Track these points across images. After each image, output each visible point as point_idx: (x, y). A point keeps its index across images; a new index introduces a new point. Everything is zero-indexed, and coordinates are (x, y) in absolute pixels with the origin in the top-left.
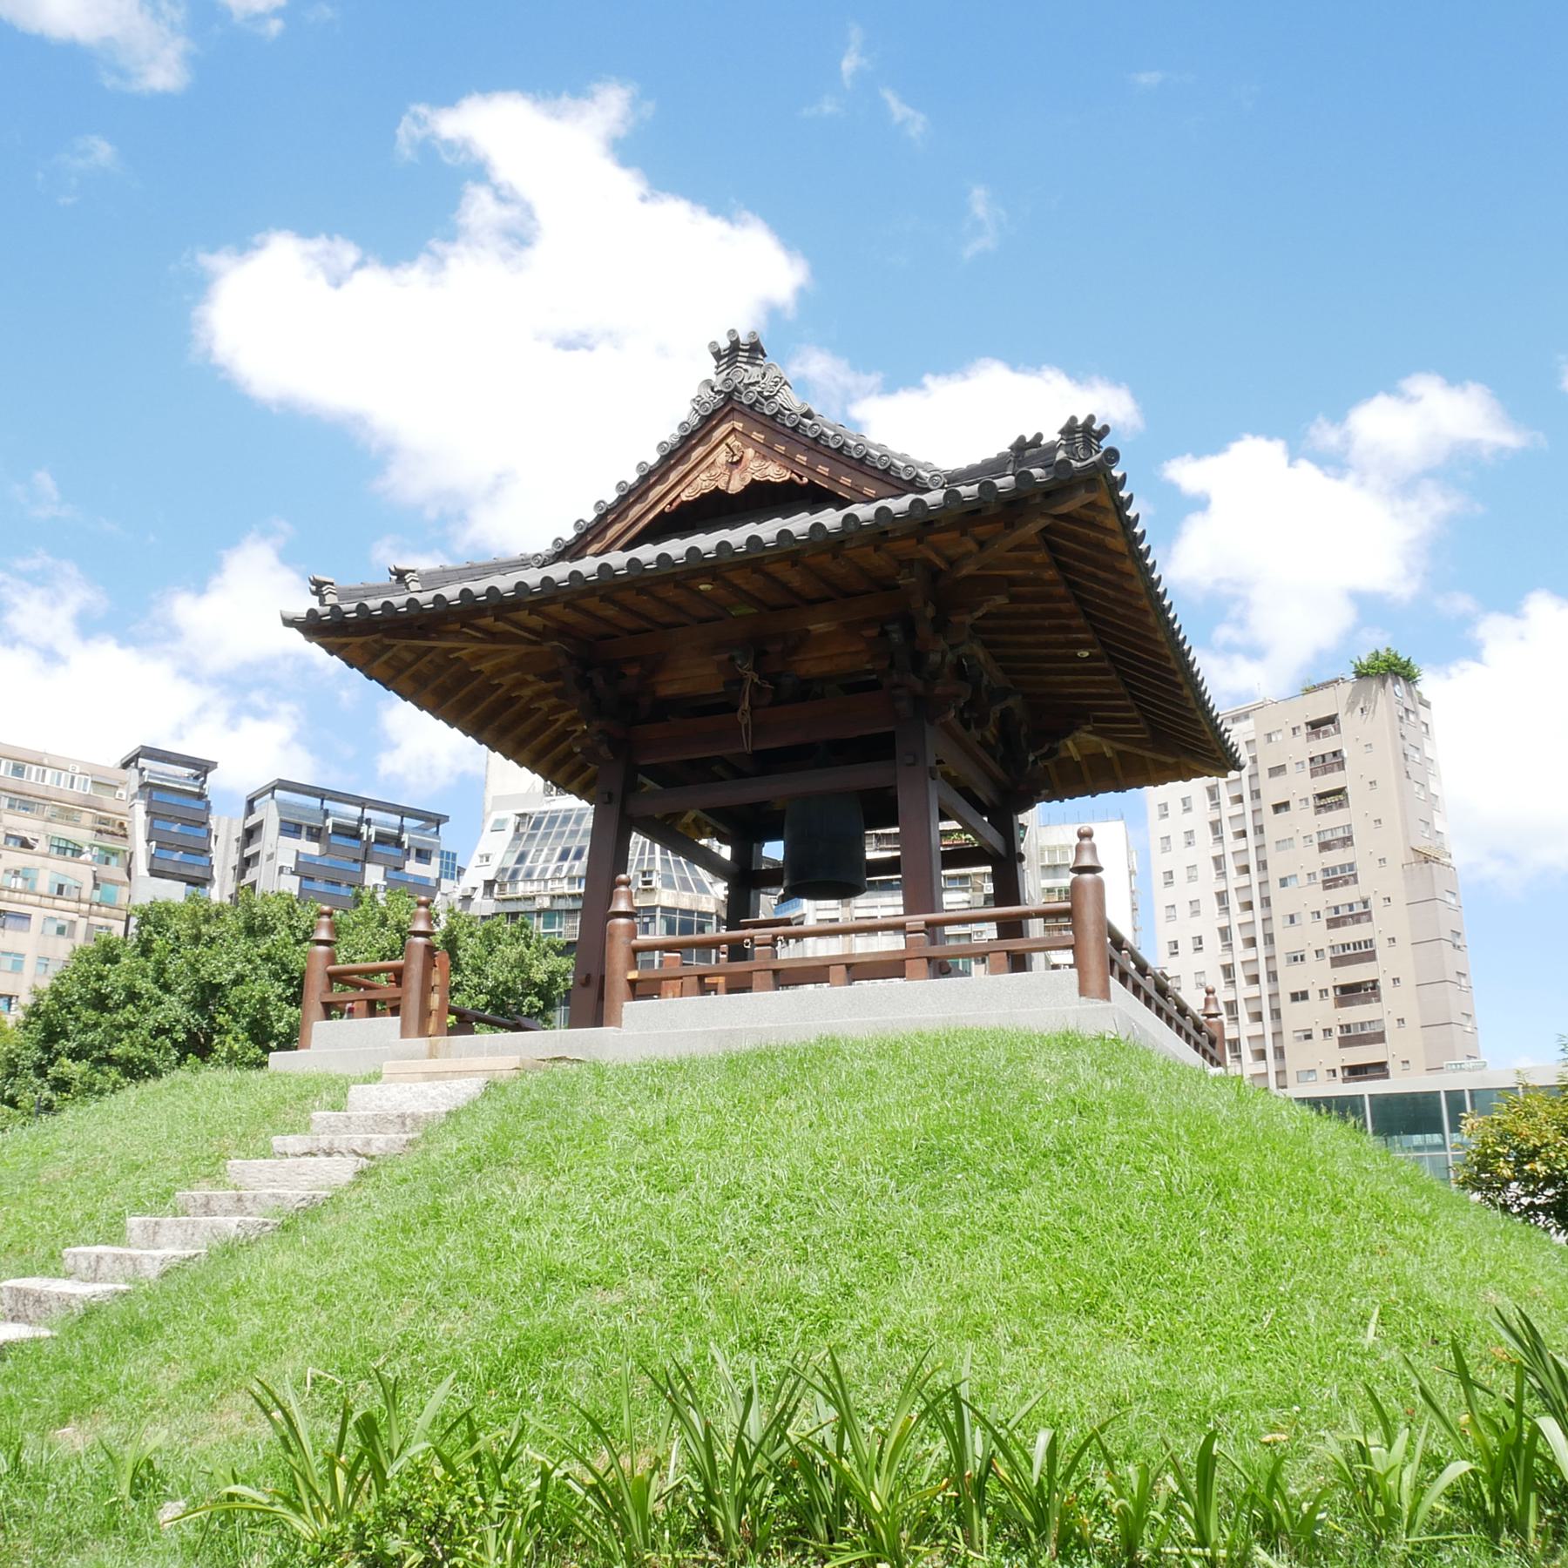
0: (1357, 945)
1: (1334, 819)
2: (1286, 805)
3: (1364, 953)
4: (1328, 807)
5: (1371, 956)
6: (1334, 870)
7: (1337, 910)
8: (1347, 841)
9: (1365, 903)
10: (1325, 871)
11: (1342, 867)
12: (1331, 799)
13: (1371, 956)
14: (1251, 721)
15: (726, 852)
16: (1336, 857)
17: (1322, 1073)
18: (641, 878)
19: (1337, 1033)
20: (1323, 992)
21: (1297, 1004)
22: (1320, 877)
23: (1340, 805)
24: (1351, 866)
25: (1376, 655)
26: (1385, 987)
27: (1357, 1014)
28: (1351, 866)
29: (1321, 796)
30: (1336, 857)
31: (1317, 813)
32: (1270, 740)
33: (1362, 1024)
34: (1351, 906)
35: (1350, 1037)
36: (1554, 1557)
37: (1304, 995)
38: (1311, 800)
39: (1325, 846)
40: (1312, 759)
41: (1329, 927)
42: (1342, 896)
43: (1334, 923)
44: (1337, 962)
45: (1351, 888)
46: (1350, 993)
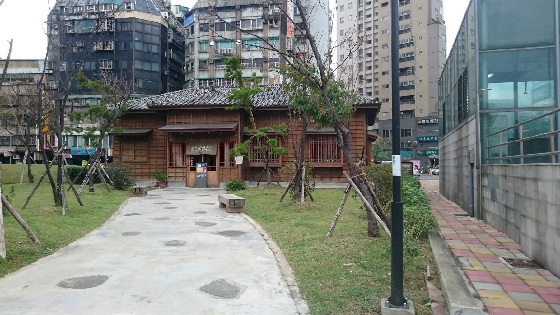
18: (126, 6)
21: (384, 76)
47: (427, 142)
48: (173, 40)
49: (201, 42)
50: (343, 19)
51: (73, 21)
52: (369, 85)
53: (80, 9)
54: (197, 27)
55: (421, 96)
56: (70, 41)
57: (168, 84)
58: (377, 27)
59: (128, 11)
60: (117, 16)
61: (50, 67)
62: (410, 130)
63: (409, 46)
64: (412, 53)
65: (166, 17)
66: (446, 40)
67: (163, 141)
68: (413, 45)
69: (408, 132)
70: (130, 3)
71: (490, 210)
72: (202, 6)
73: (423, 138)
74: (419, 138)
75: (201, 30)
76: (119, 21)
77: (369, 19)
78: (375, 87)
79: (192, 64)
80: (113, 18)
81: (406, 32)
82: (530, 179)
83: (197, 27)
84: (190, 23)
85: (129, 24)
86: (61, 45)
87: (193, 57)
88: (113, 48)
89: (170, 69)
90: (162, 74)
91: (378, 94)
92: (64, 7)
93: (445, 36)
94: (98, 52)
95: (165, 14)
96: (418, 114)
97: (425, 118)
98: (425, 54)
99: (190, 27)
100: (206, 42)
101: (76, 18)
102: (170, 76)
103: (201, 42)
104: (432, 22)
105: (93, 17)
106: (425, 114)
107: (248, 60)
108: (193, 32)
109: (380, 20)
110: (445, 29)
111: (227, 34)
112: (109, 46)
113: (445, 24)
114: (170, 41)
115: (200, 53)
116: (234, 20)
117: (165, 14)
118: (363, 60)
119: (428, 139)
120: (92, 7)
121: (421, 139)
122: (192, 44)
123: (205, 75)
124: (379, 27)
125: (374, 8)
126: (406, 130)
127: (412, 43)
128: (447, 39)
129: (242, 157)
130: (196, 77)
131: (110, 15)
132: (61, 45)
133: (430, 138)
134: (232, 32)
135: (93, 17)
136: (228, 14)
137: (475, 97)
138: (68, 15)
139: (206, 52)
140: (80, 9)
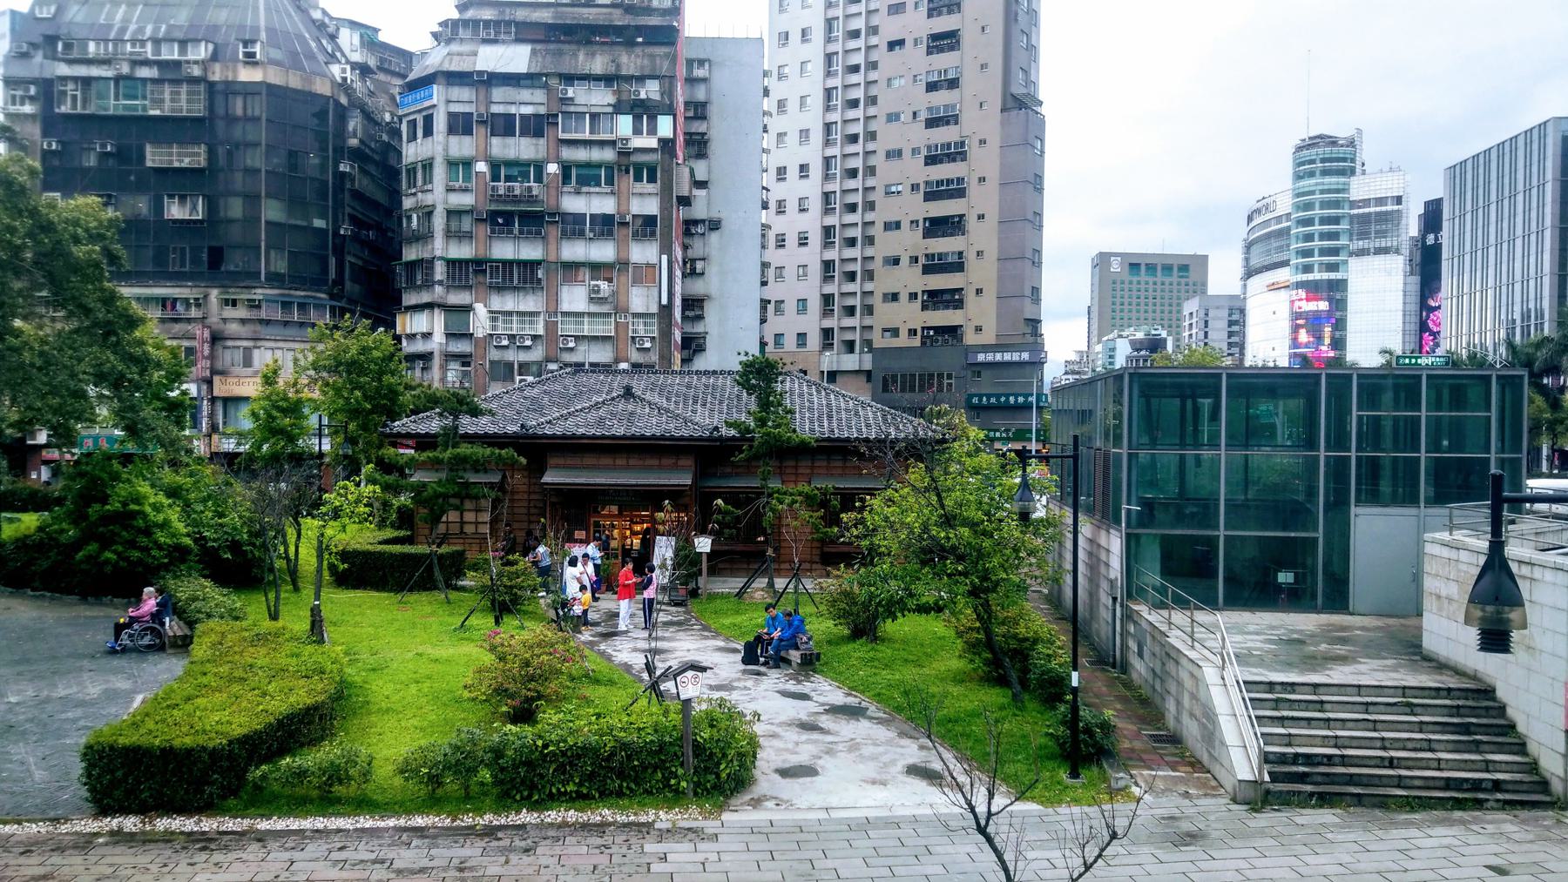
0: (950, 181)
1: (945, 61)
2: (901, 43)
4: (940, 50)
5: (959, 304)
8: (953, 84)
9: (963, 144)
10: (927, 183)
13: (959, 304)
15: (210, 544)
16: (942, 98)
18: (241, 50)
19: (922, 260)
21: (897, 147)
23: (952, 48)
26: (971, 223)
27: (944, 245)
29: (935, 37)
31: (929, 53)
32: (889, 85)
35: (935, 265)
36: (1071, 494)
37: (898, 225)
39: (932, 87)
41: (926, 164)
44: (930, 196)
45: (952, 128)
46: (938, 226)
47: (989, 408)
48: (361, 141)
49: (452, 164)
50: (786, 70)
51: (86, 82)
52: (849, 253)
53: (106, 49)
54: (440, 123)
55: (979, 291)
57: (349, 258)
58: (873, 101)
59: (246, 63)
60: (217, 74)
62: (950, 377)
63: (954, 160)
64: (960, 180)
65: (345, 79)
66: (1042, 152)
68: (964, 160)
69: (946, 381)
70: (253, 42)
72: (454, 67)
73: (980, 396)
74: (971, 396)
76: (219, 87)
77: (854, 78)
78: (864, 293)
81: (948, 123)
82: (1497, 546)
83: (440, 123)
85: (249, 98)
86: (50, 144)
87: (428, 199)
88: (202, 161)
89: (354, 220)
90: (336, 234)
91: (871, 278)
93: (1042, 141)
95: (344, 71)
96: (970, 338)
97: (986, 348)
98: (993, 184)
100: (468, 164)
101: (95, 71)
102: (355, 238)
103: (452, 164)
104: (1010, 104)
105: (144, 72)
106: (988, 337)
107: (579, 218)
108: (428, 132)
109: (883, 83)
110: (1043, 122)
111: (522, 148)
112: (190, 157)
113: (1044, 110)
114: (354, 142)
115: (450, 190)
116: (542, 110)
117: (344, 71)
118: (834, 151)
119: (993, 400)
120: (143, 46)
121: (975, 400)
122: (428, 165)
123: (463, 251)
124: (879, 101)
125: (867, 118)
126: (940, 376)
128: (1047, 149)
130: (438, 253)
131: (197, 71)
132: (50, 144)
134: (534, 140)
135: (144, 72)
136: (525, 94)
138: (71, 62)
139: (466, 190)
140: (106, 49)
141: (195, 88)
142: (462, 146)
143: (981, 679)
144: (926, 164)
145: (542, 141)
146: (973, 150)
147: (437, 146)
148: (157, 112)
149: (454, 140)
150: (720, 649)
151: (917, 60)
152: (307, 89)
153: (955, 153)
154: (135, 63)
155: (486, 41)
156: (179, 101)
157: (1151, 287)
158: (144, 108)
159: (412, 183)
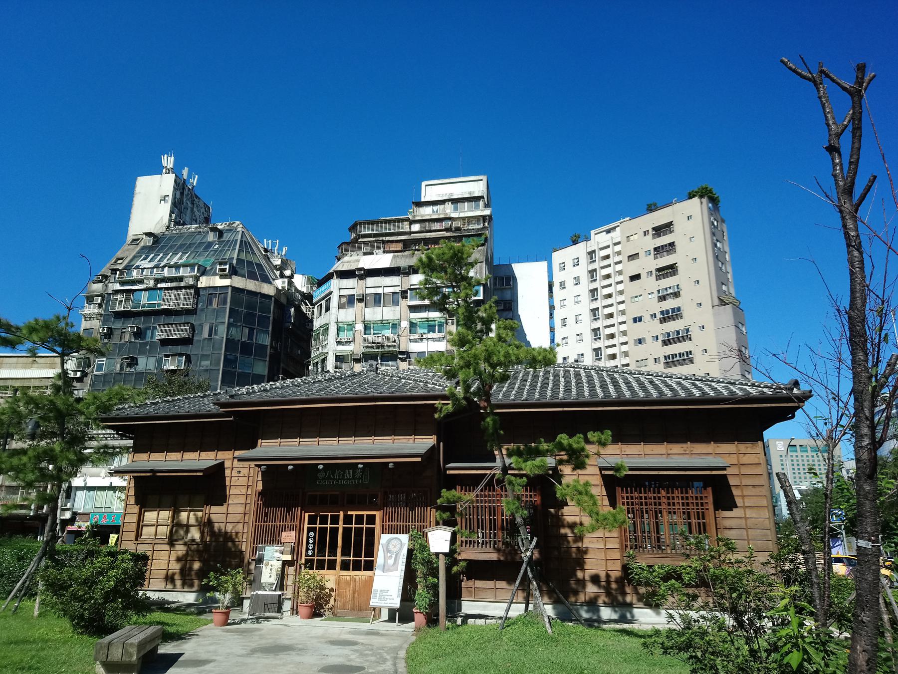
3: (684, 336)
4: (665, 276)
5: (691, 361)
6: (668, 312)
7: (669, 334)
8: (676, 295)
9: (688, 330)
10: (662, 313)
11: (673, 310)
12: (670, 270)
14: (520, 270)
16: (670, 304)
17: (651, 361)
19: (663, 360)
20: (654, 316)
22: (659, 316)
23: (673, 274)
24: (679, 309)
25: (36, 320)
28: (679, 309)
29: (659, 270)
30: (670, 304)
33: (666, 289)
34: (678, 332)
38: (654, 272)
40: (659, 291)
41: (663, 345)
42: (672, 326)
43: (666, 343)
56: (117, 325)
61: (79, 366)
63: (683, 341)
67: (244, 491)
71: (592, 595)
75: (341, 306)
79: (324, 360)
80: (194, 287)
84: (323, 295)
92: (118, 270)
94: (164, 343)
99: (324, 302)
108: (328, 309)
115: (339, 343)
116: (397, 289)
117: (284, 282)
122: (326, 329)
127: (687, 336)
129: (450, 534)
133: (482, 319)
137: (658, 205)
141: (188, 291)
142: (347, 315)
143: (81, 617)
144: (663, 345)
145: (398, 308)
146: (694, 332)
147: (335, 315)
148: (166, 307)
149: (342, 311)
150: (172, 625)
151: (650, 284)
152: (258, 291)
153: (684, 336)
154: (157, 281)
155: (365, 254)
156: (179, 299)
157: (805, 458)
158: (159, 304)
159: (318, 343)
